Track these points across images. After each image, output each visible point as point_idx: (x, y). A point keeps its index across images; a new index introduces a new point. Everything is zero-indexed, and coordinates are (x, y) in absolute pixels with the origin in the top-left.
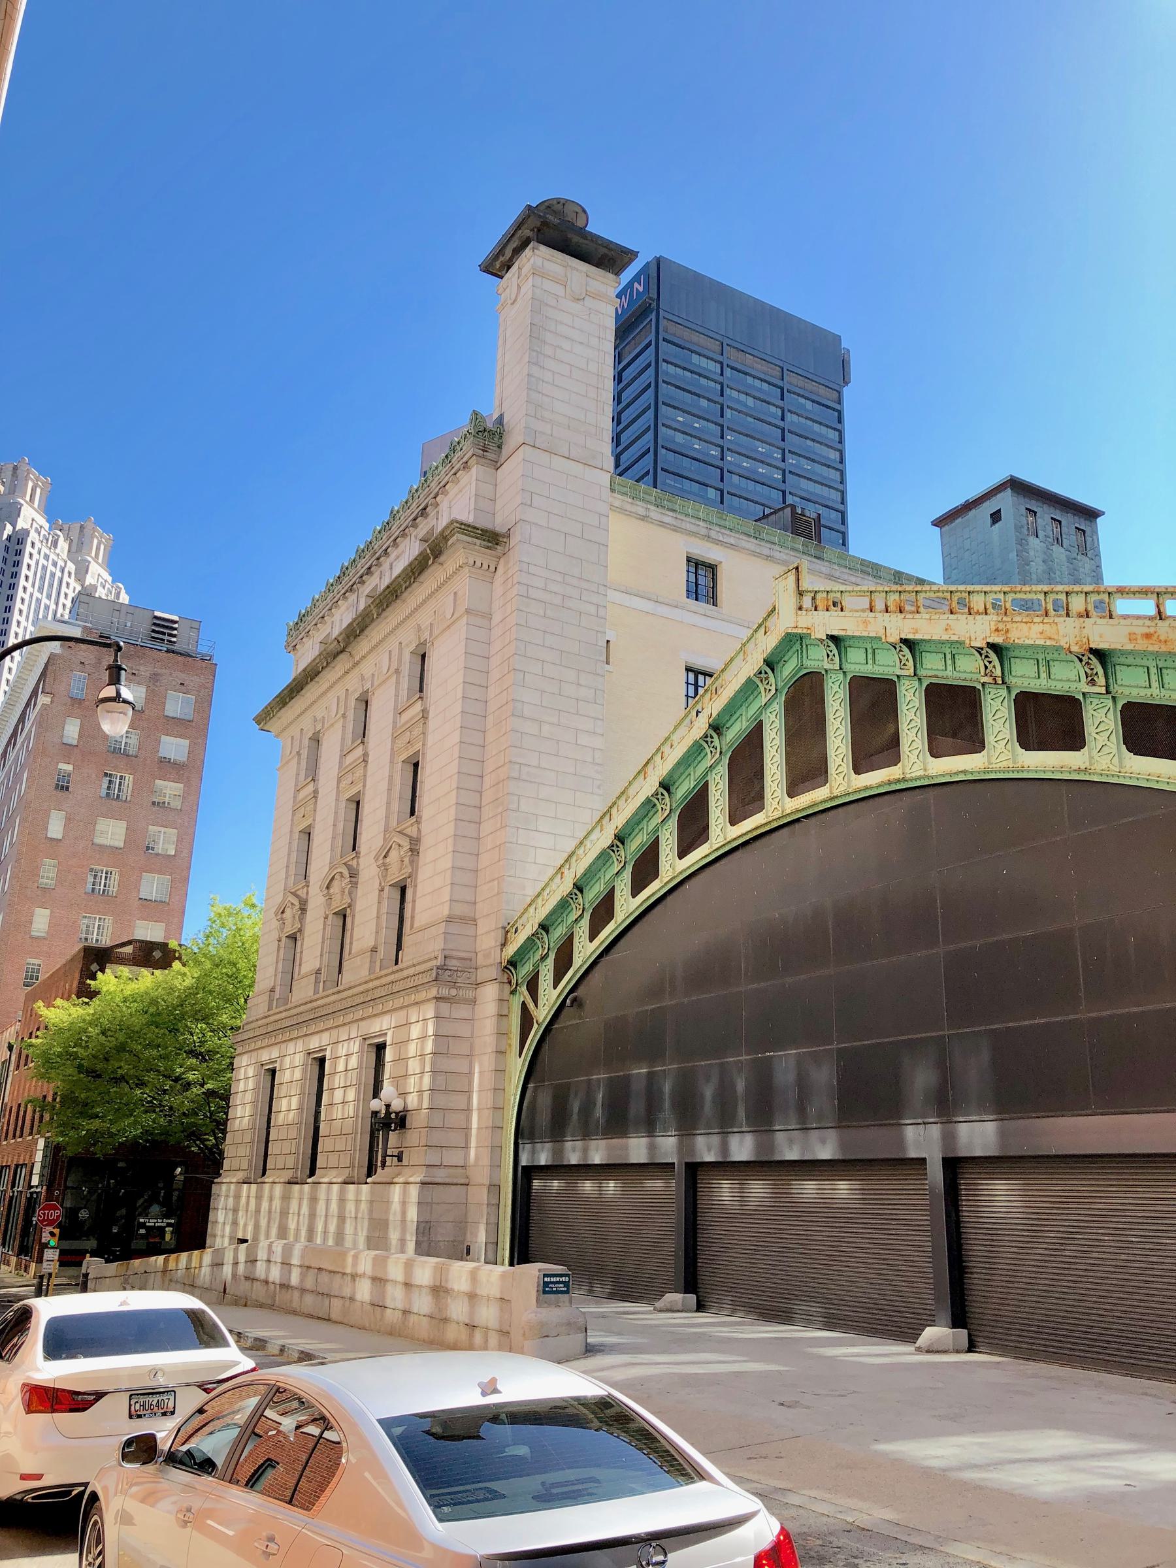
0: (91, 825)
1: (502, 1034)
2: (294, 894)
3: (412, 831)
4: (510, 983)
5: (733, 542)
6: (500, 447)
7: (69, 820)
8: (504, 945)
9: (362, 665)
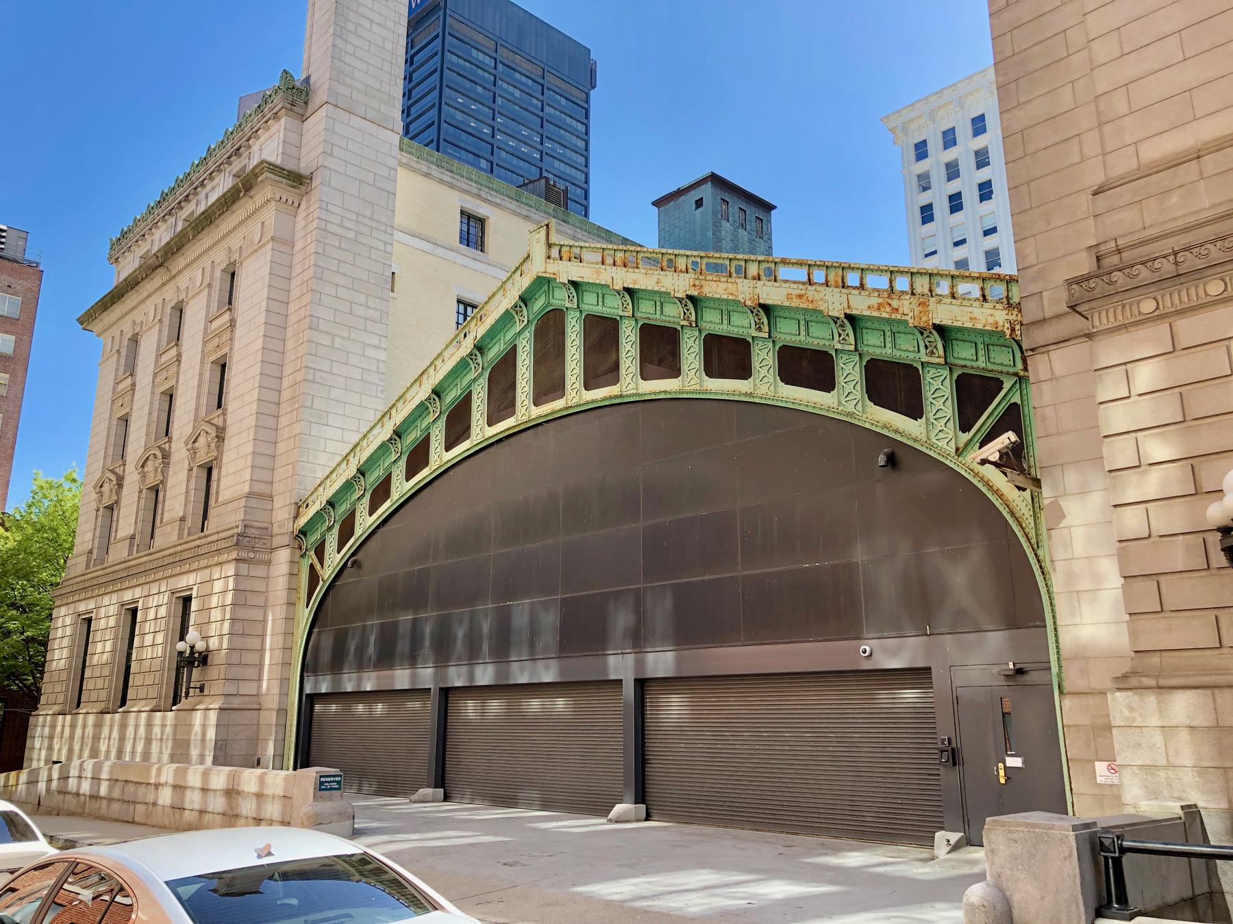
1: (292, 589)
2: (112, 471)
3: (119, 471)
8: (296, 518)
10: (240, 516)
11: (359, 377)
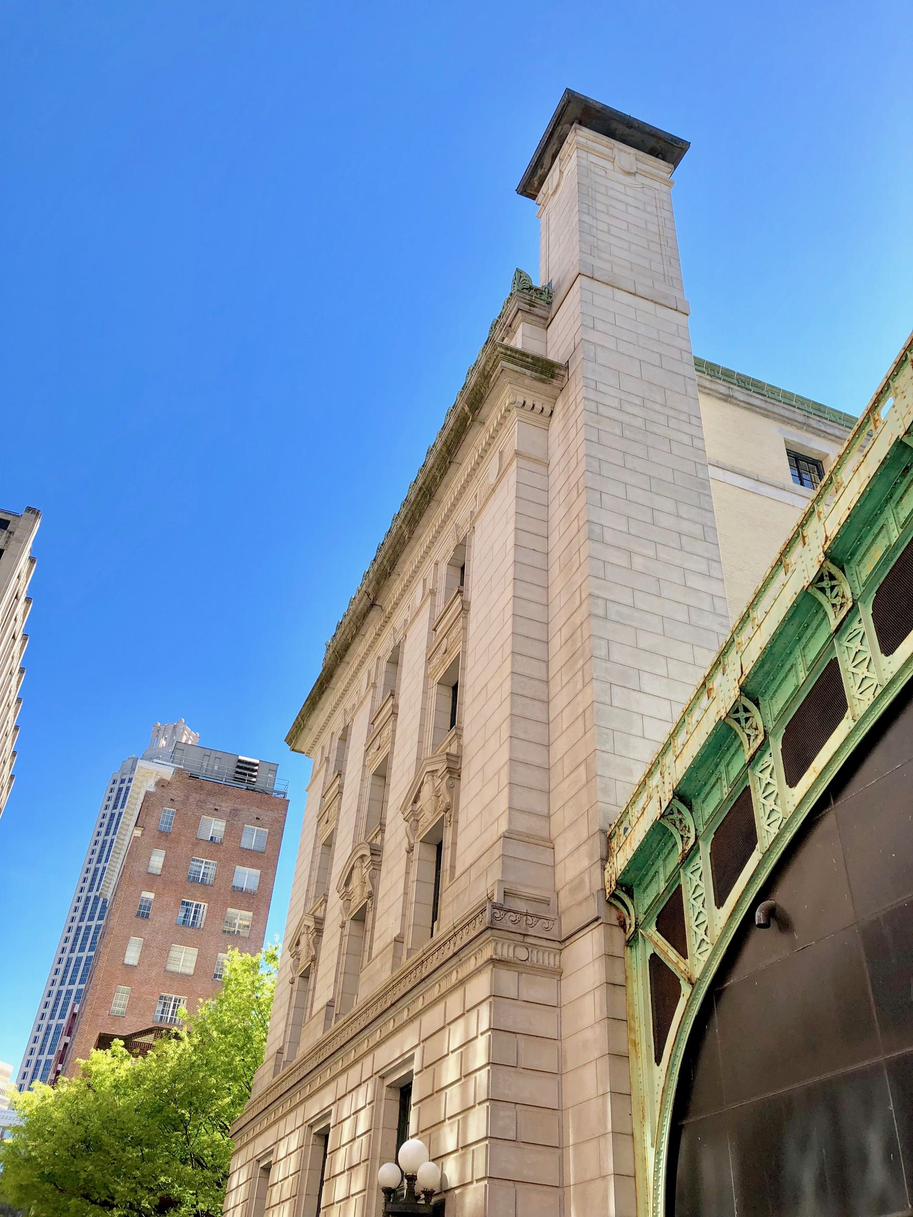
0: (165, 952)
1: (617, 1020)
4: (623, 925)
5: (837, 433)
6: (549, 303)
7: (146, 946)
8: (605, 859)
9: (393, 620)
10: (496, 874)
11: (684, 618)
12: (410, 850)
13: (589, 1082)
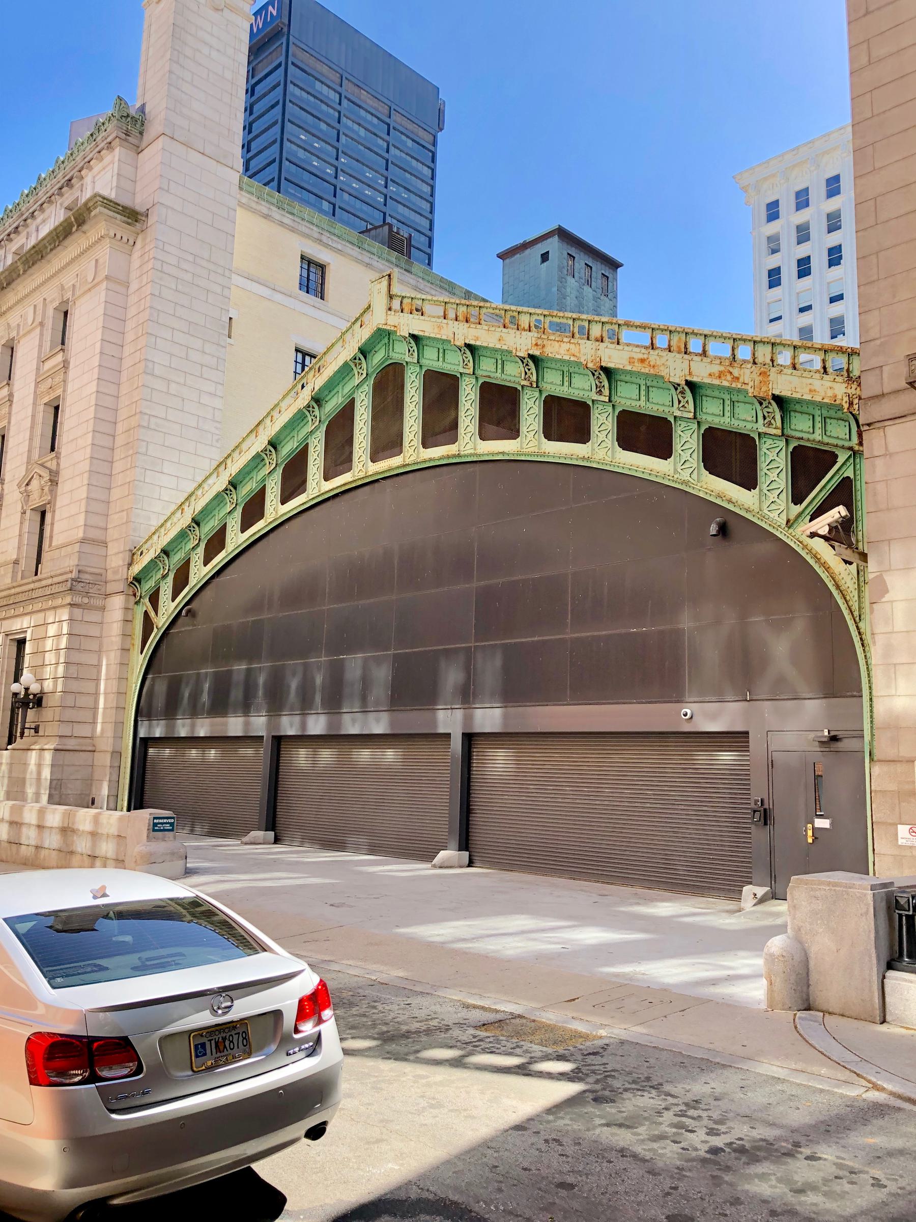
1: (126, 635)
4: (135, 595)
12: (24, 513)
13: (107, 666)
